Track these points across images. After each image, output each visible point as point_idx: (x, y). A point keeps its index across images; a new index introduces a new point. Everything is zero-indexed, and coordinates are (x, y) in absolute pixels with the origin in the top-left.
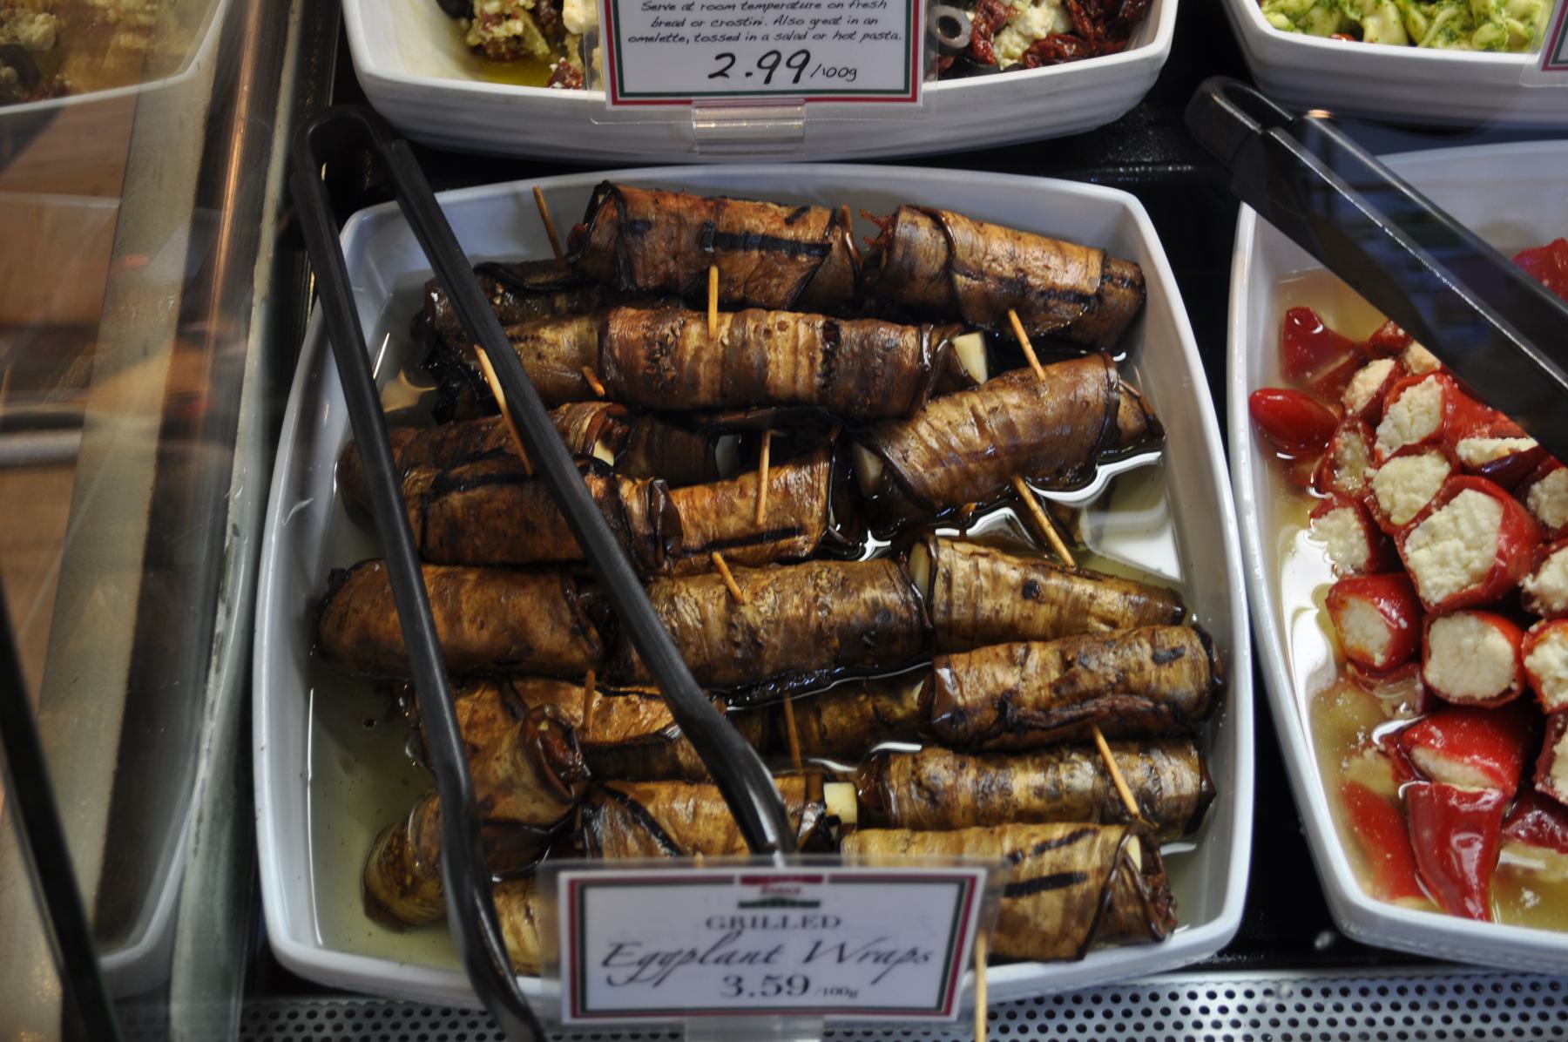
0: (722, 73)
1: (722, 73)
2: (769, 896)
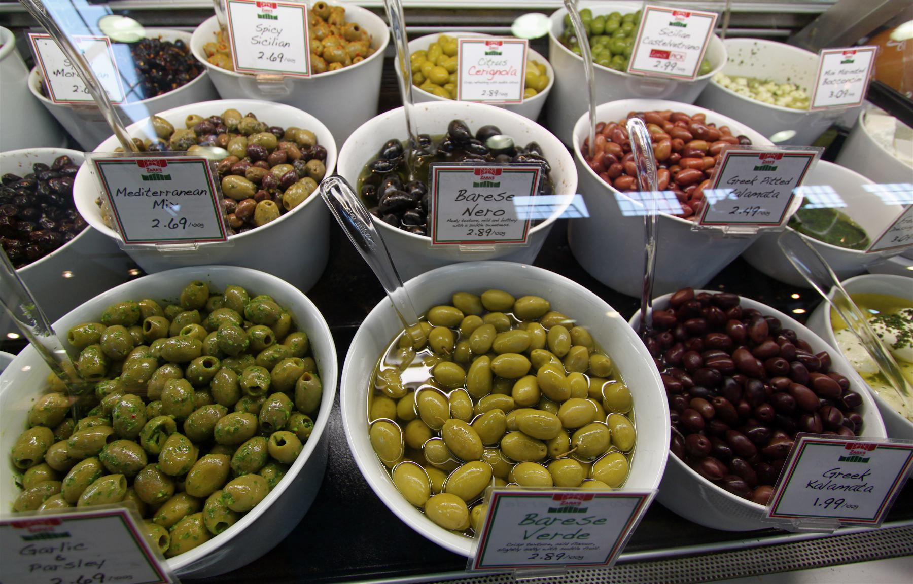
0: (156, 226)
1: (156, 226)
2: (564, 506)
